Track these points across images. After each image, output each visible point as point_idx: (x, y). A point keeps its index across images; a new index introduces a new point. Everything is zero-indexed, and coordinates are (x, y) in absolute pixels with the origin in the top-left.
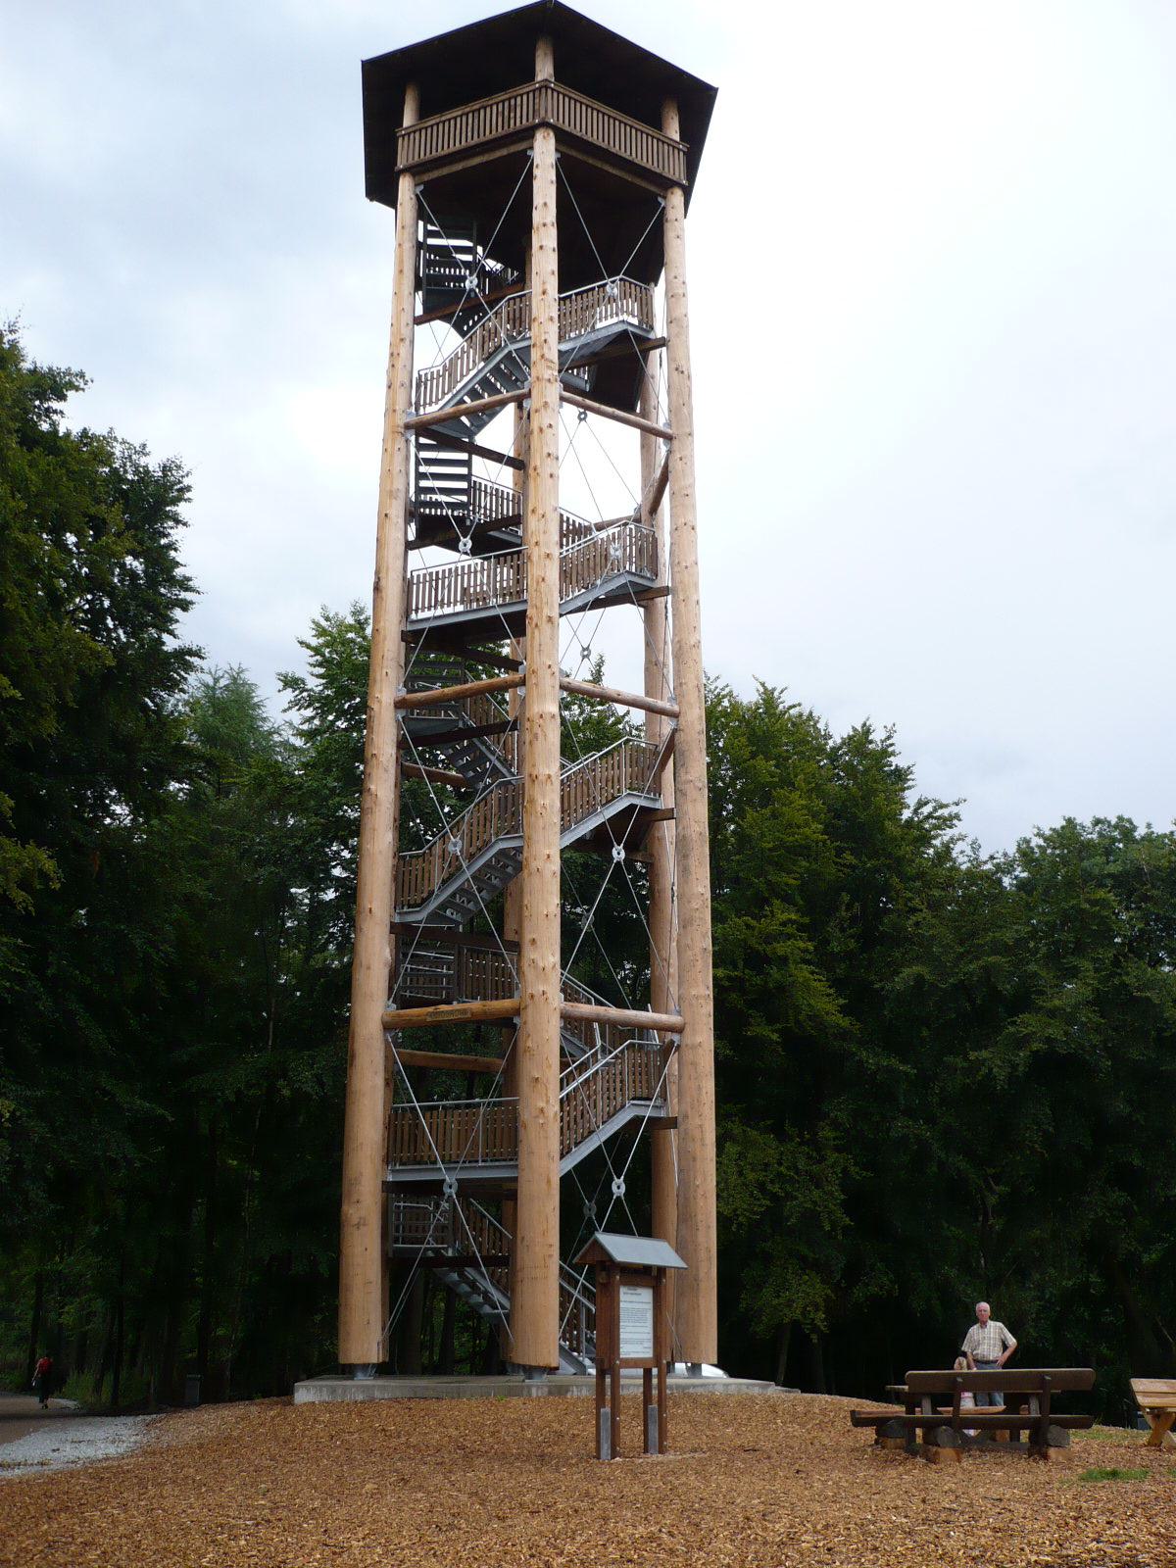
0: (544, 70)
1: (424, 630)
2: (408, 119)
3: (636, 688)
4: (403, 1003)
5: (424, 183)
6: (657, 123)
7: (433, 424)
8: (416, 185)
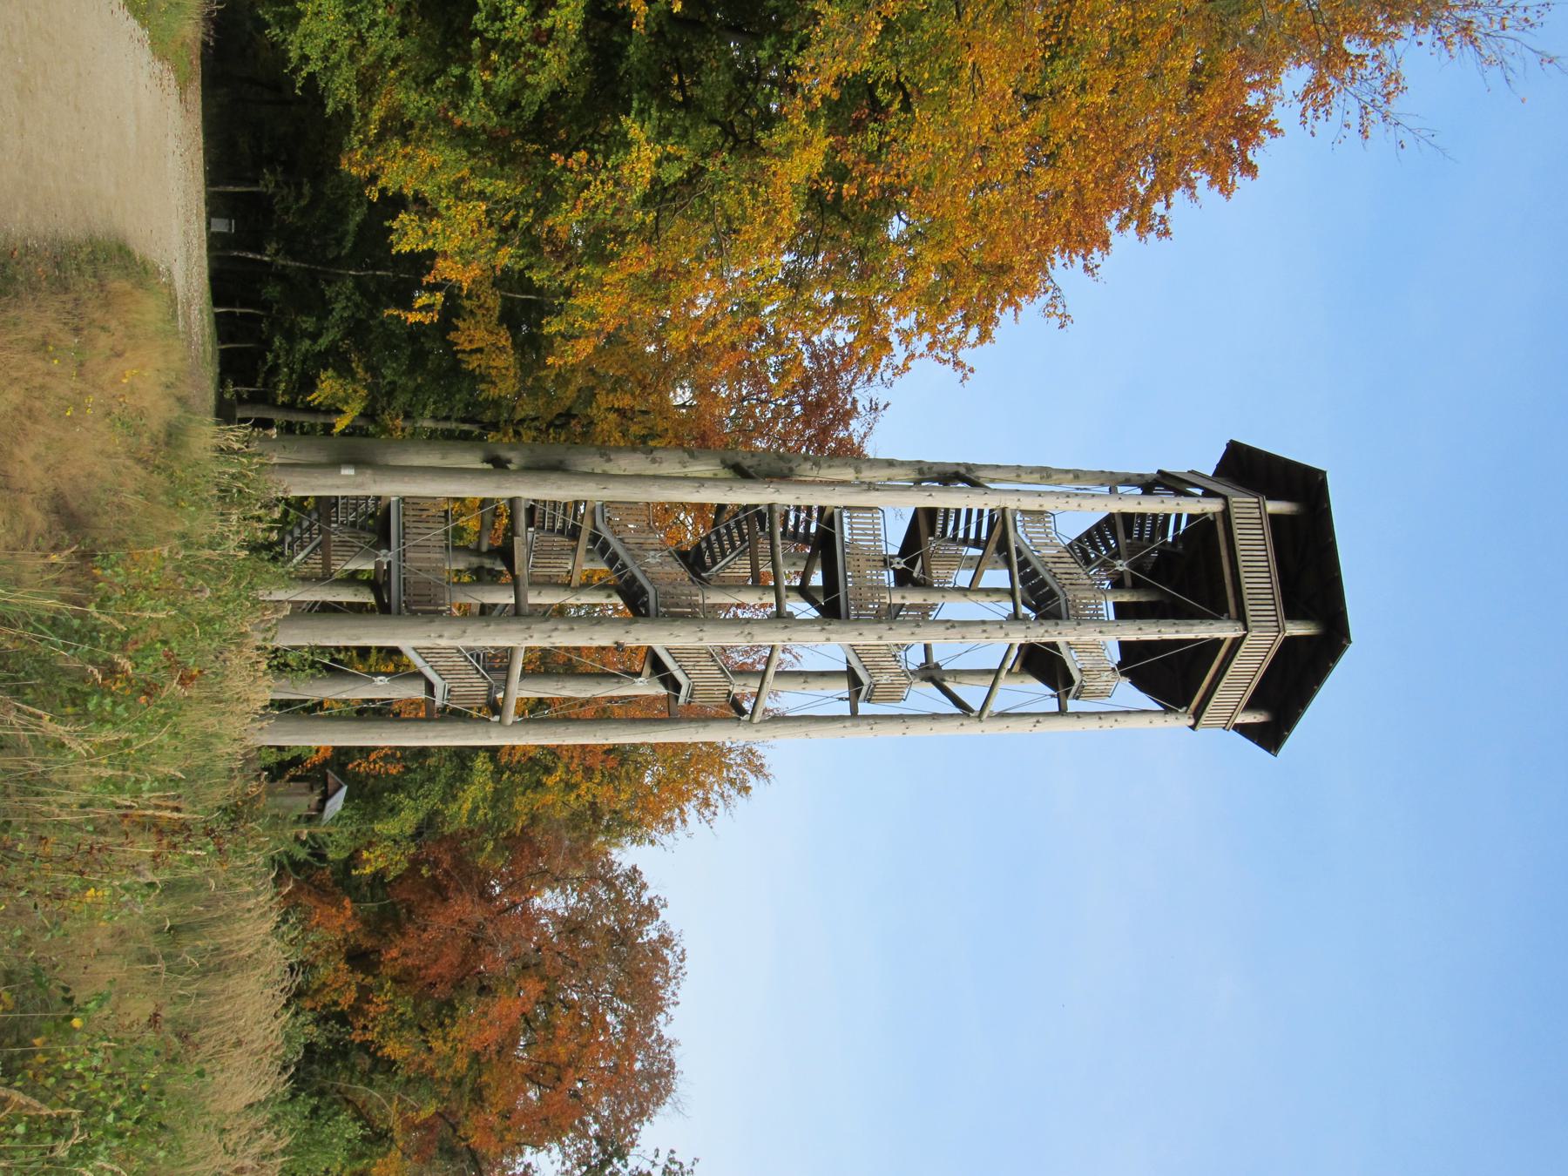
0: (1297, 629)
1: (833, 528)
2: (1273, 507)
3: (767, 702)
4: (531, 511)
5: (1215, 521)
6: (1251, 706)
7: (952, 715)
8: (1214, 514)
